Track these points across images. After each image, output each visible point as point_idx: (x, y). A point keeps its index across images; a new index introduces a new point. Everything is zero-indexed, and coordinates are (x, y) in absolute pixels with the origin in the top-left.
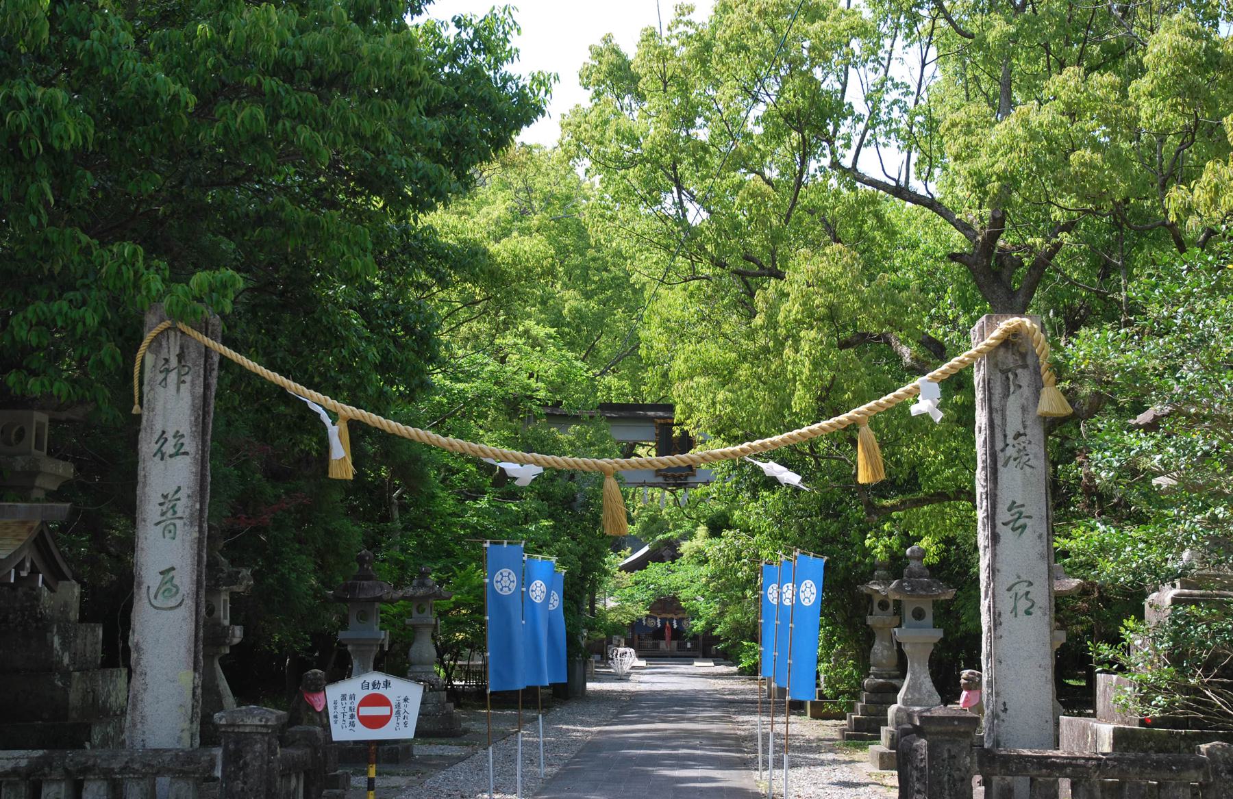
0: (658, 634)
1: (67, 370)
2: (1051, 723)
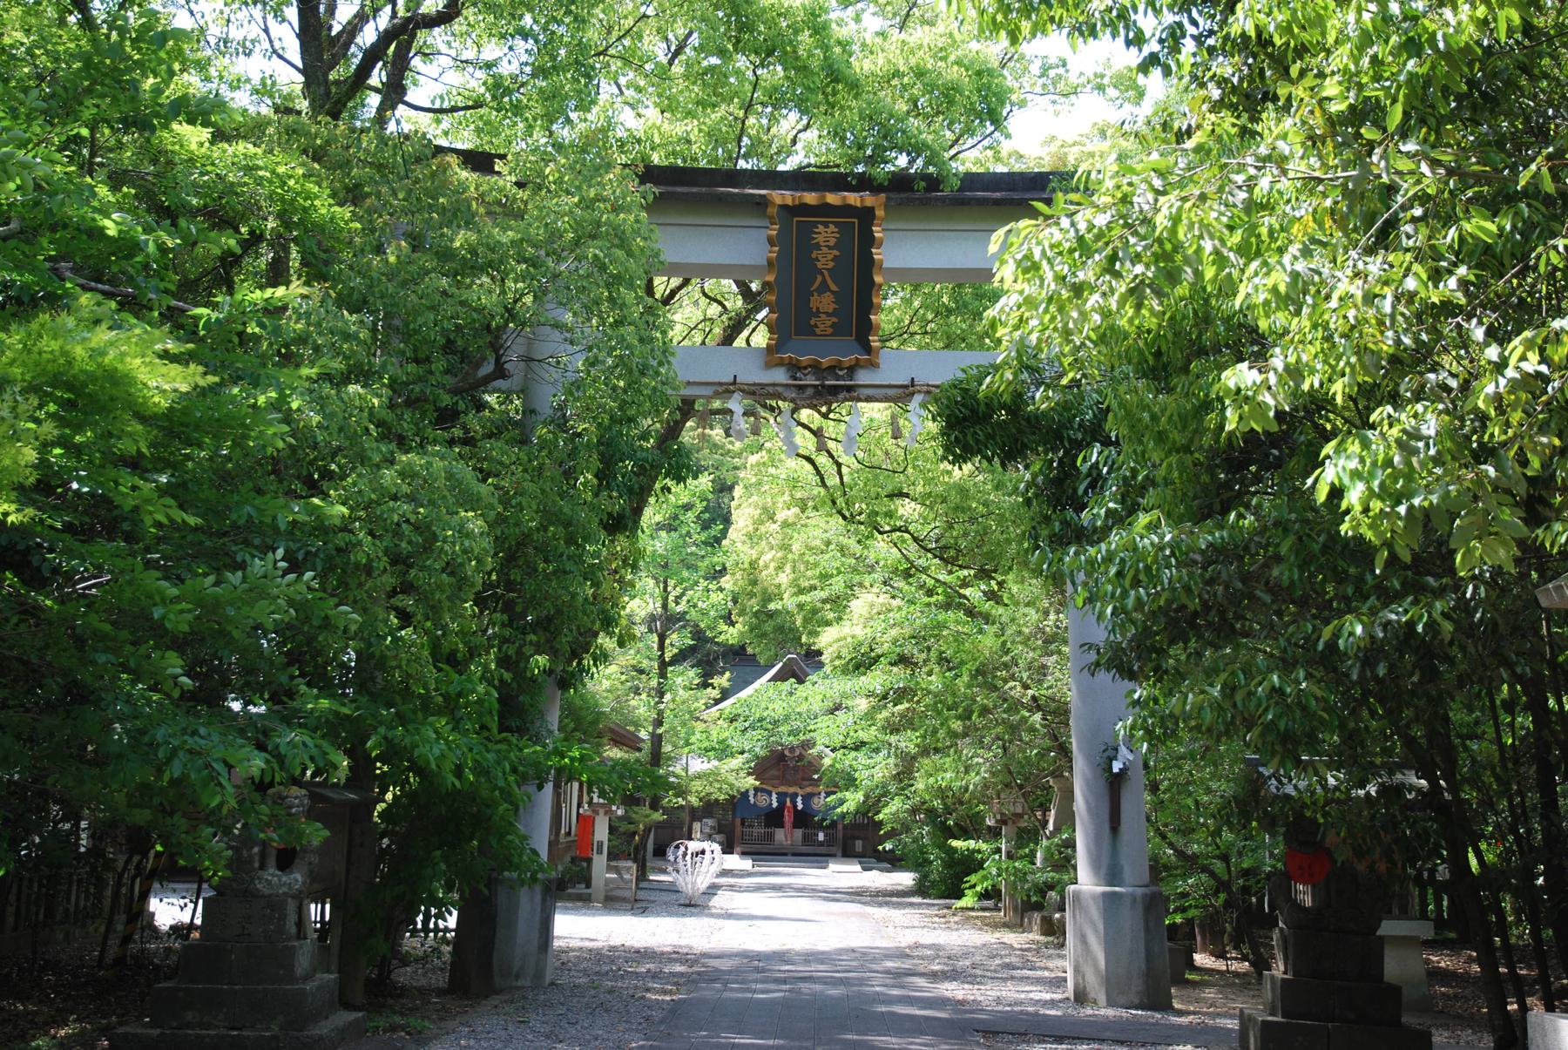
0: (774, 818)
1: (215, 874)
2: (721, 922)
